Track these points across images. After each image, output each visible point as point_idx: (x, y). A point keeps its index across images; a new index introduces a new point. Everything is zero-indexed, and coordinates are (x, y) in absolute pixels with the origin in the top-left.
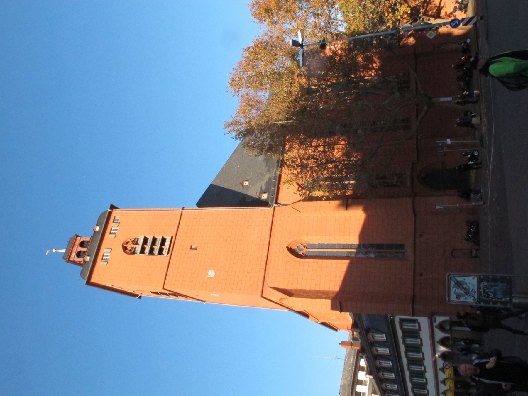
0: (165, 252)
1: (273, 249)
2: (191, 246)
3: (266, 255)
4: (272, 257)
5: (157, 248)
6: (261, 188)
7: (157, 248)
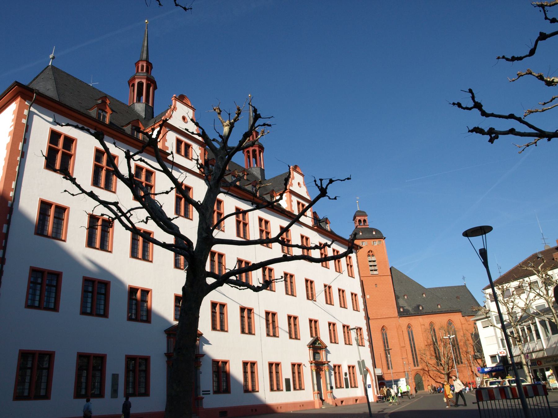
0: (371, 272)
1: (382, 320)
2: (376, 284)
3: (380, 318)
4: (379, 320)
5: (373, 268)
6: (405, 307)
7: (373, 268)
